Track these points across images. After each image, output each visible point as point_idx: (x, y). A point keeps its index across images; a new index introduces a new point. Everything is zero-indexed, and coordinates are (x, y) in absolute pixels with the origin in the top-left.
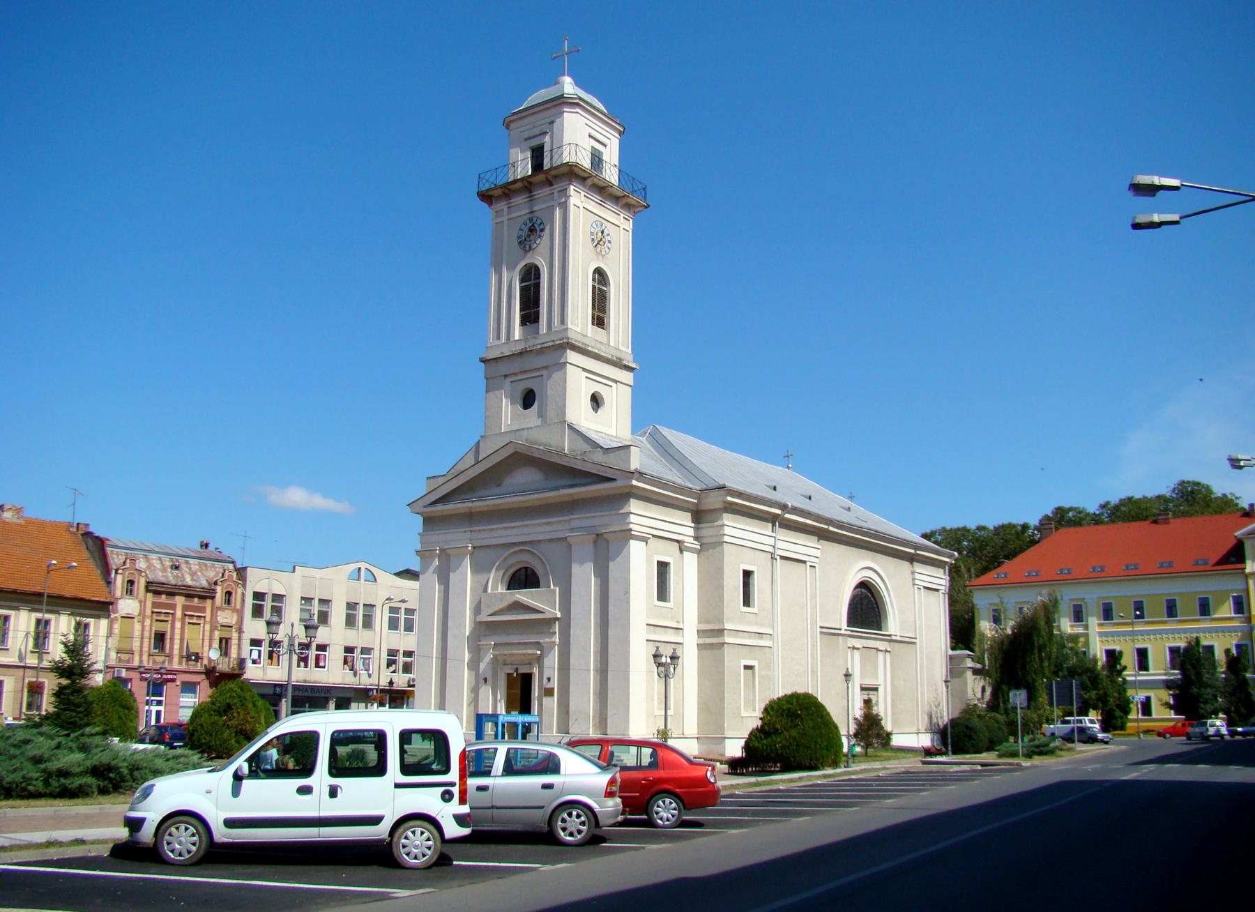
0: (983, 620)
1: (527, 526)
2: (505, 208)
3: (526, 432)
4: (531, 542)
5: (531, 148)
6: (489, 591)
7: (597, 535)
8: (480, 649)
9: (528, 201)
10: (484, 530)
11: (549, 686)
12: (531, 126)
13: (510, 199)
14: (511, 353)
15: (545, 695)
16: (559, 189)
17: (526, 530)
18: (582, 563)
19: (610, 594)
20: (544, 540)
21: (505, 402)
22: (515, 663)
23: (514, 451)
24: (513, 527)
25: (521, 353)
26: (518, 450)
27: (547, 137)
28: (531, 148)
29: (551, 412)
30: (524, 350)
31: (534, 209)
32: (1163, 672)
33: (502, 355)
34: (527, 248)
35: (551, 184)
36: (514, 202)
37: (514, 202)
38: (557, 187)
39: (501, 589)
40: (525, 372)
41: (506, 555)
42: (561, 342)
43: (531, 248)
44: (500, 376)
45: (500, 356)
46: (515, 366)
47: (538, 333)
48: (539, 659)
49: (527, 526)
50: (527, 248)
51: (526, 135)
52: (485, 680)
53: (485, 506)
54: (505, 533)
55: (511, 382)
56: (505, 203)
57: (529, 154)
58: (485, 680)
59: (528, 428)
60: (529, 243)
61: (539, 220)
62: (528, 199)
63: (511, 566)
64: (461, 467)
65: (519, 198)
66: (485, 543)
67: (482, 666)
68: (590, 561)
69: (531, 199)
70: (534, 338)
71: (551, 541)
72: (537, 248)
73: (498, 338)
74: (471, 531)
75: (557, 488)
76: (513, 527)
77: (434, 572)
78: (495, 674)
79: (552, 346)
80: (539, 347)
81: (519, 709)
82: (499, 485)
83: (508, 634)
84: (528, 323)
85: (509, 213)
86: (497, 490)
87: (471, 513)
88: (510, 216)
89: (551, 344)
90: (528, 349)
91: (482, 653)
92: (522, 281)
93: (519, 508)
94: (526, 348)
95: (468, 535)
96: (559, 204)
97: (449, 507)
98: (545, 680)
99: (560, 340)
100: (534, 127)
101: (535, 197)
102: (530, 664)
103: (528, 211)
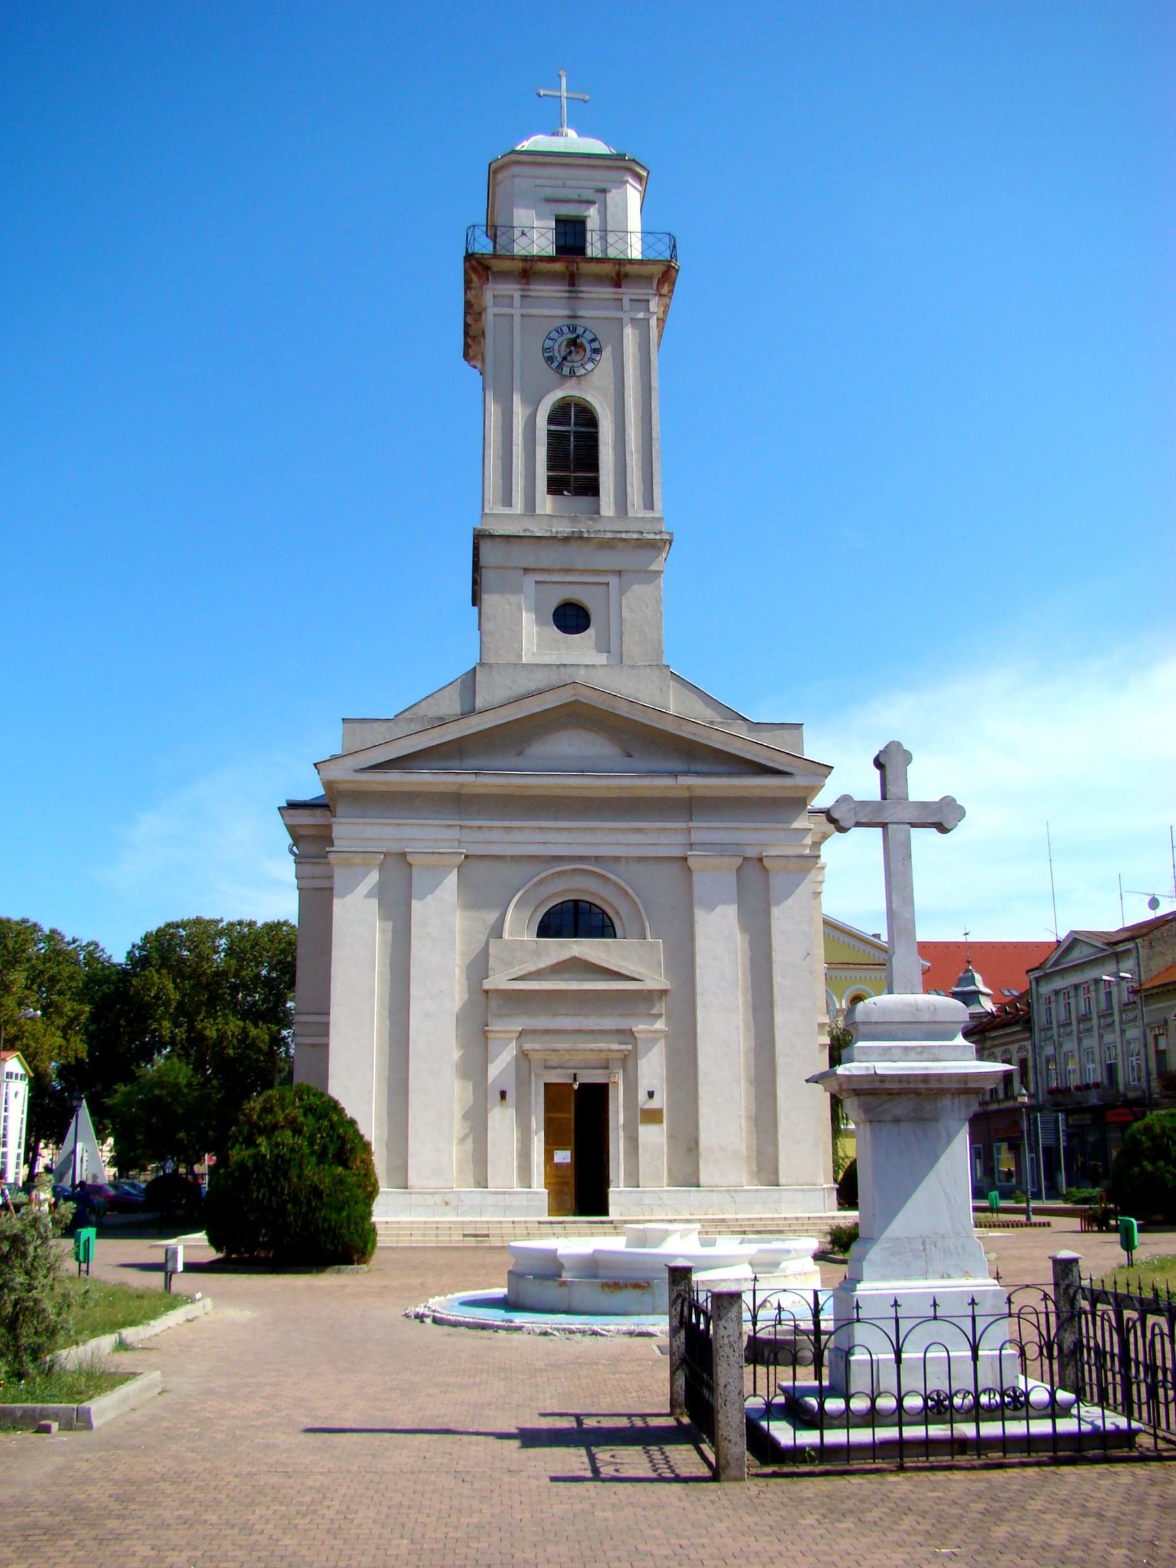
0: (568, 1164)
1: (592, 829)
2: (517, 296)
3: (582, 671)
4: (597, 859)
5: (556, 216)
6: (506, 936)
7: (745, 859)
8: (486, 1038)
9: (565, 298)
10: (490, 828)
11: (654, 1104)
12: (560, 183)
13: (528, 284)
14: (548, 534)
15: (642, 1122)
16: (634, 297)
17: (589, 838)
18: (711, 907)
19: (777, 956)
20: (626, 858)
21: (528, 620)
22: (571, 1064)
23: (573, 699)
24: (560, 829)
25: (566, 539)
26: (581, 699)
27: (592, 209)
28: (556, 216)
29: (632, 647)
30: (576, 535)
31: (580, 313)
32: (500, 1291)
33: (528, 534)
34: (566, 371)
35: (618, 285)
36: (536, 290)
37: (536, 290)
38: (628, 293)
39: (529, 937)
40: (568, 571)
41: (543, 875)
42: (658, 537)
43: (572, 373)
44: (516, 568)
45: (522, 534)
46: (551, 557)
47: (598, 512)
48: (628, 1062)
49: (592, 829)
50: (566, 371)
51: (548, 192)
52: (503, 1095)
53: (493, 786)
54: (540, 837)
55: (536, 582)
56: (519, 287)
57: (553, 224)
58: (503, 1095)
59: (587, 666)
60: (570, 364)
61: (551, 336)
62: (567, 295)
63: (555, 895)
64: (432, 710)
65: (548, 288)
66: (495, 850)
67: (494, 1070)
68: (725, 902)
69: (574, 296)
70: (590, 519)
71: (641, 859)
72: (587, 377)
73: (507, 501)
74: (461, 827)
75: (675, 774)
76: (560, 829)
77: (368, 896)
78: (523, 1083)
79: (638, 539)
80: (610, 535)
81: (573, 1146)
82: (520, 754)
83: (555, 1015)
84: (565, 493)
85: (522, 306)
86: (518, 762)
87: (460, 795)
88: (525, 311)
89: (635, 536)
90: (586, 536)
91: (492, 1046)
92: (552, 420)
93: (576, 798)
94: (581, 532)
95: (455, 833)
96: (632, 319)
97: (396, 779)
98: (642, 1095)
99: (655, 533)
100: (564, 186)
101: (581, 295)
102: (607, 1068)
103: (567, 313)
